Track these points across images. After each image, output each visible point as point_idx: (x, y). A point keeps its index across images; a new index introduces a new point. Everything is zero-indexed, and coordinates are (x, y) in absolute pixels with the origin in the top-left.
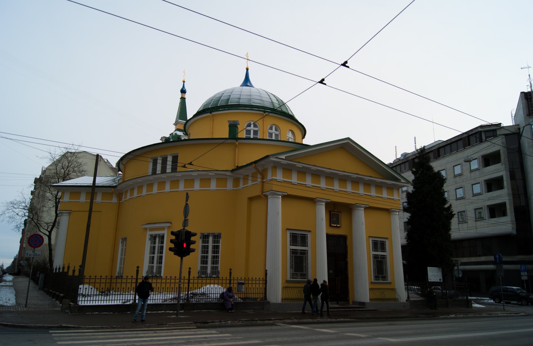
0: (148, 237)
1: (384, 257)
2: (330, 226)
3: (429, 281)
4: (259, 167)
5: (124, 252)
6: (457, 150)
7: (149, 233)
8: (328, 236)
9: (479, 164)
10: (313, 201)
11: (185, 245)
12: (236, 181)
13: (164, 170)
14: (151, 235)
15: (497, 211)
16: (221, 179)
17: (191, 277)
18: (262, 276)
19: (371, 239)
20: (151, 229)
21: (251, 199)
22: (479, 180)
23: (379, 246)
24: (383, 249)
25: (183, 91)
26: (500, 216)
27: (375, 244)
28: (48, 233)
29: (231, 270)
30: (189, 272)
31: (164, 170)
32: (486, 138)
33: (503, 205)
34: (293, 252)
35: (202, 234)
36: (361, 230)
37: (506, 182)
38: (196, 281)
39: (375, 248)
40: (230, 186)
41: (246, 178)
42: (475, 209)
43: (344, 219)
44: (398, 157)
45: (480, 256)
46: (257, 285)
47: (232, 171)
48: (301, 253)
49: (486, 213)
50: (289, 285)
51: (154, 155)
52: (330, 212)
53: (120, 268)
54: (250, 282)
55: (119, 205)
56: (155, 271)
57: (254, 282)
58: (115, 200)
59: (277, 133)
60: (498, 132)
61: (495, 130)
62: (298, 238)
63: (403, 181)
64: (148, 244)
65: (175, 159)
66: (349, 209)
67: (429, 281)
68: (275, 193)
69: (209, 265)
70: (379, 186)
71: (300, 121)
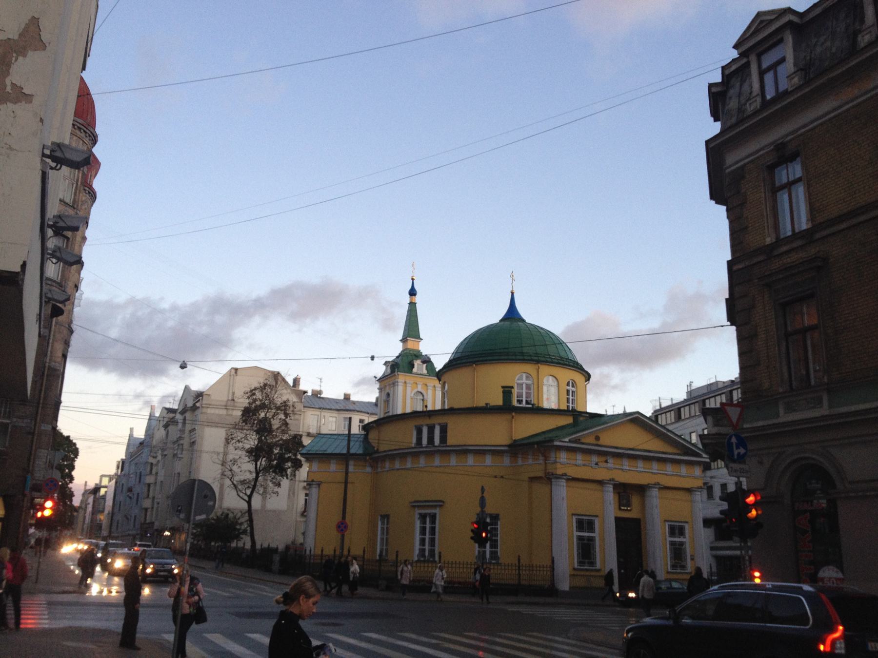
0: (417, 516)
2: (620, 509)
4: (541, 445)
5: (386, 531)
7: (418, 511)
8: (618, 520)
10: (601, 483)
11: (484, 535)
14: (420, 514)
16: (496, 452)
18: (549, 563)
21: (532, 479)
23: (677, 531)
25: (412, 292)
28: (246, 498)
31: (431, 440)
34: (580, 538)
36: (659, 512)
43: (635, 500)
47: (509, 446)
48: (584, 563)
50: (576, 573)
56: (427, 554)
62: (585, 524)
64: (418, 524)
66: (641, 490)
69: (427, 547)
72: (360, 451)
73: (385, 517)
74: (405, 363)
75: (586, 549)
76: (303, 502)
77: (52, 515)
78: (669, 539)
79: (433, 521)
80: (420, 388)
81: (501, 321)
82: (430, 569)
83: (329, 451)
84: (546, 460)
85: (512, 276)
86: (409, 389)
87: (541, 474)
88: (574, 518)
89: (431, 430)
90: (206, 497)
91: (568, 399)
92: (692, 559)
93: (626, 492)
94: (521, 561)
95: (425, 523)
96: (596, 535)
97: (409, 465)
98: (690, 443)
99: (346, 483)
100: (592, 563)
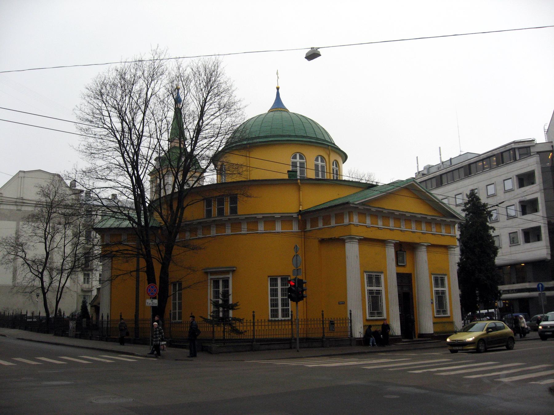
1: (379, 292)
3: (157, 305)
6: (491, 168)
7: (210, 277)
8: (398, 274)
9: (513, 185)
10: (383, 242)
15: (531, 235)
17: (256, 320)
19: (433, 276)
22: (513, 202)
23: (439, 282)
26: (535, 241)
29: (254, 312)
30: (254, 316)
31: (221, 212)
32: (520, 155)
33: (538, 229)
37: (541, 205)
39: (370, 283)
40: (295, 228)
42: (510, 234)
43: (407, 257)
44: (420, 170)
45: (514, 283)
46: (263, 327)
54: (263, 324)
57: (260, 324)
60: (532, 150)
61: (529, 147)
67: (157, 305)
68: (352, 238)
71: (342, 149)
75: (375, 301)
77: (494, 263)
78: (434, 289)
81: (271, 111)
82: (283, 327)
93: (405, 250)
94: (325, 316)
95: (218, 287)
96: (382, 288)
97: (403, 228)
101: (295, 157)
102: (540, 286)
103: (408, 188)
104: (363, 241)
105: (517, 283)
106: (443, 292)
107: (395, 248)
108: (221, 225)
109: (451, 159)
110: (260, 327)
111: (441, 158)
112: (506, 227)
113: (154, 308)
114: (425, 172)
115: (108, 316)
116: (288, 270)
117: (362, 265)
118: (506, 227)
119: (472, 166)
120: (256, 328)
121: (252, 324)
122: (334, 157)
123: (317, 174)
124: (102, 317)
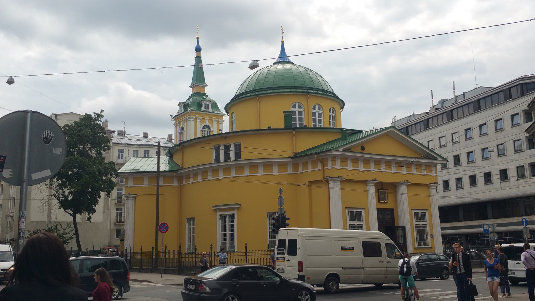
0: (218, 217)
1: (424, 226)
2: (379, 202)
4: (318, 155)
6: (499, 103)
7: (219, 213)
8: (378, 210)
12: (296, 166)
13: (227, 157)
14: (221, 215)
16: (282, 165)
17: (213, 253)
20: (220, 210)
23: (420, 217)
24: (424, 219)
25: (198, 50)
27: (417, 215)
29: (246, 244)
30: (246, 247)
31: (227, 157)
35: (268, 213)
38: (266, 253)
39: (417, 219)
40: (290, 171)
41: (305, 165)
43: (390, 197)
47: (292, 158)
49: (527, 171)
51: (217, 143)
52: (378, 190)
53: (189, 245)
55: (181, 187)
57: (251, 254)
58: (175, 183)
59: (320, 111)
63: (439, 159)
65: (238, 147)
66: (394, 186)
67: (49, 170)
68: (334, 179)
70: (419, 166)
72: (167, 169)
73: (191, 220)
74: (197, 103)
76: (116, 214)
79: (232, 221)
80: (207, 123)
83: (142, 170)
84: (324, 167)
85: (282, 28)
86: (199, 123)
87: (320, 178)
88: (347, 211)
89: (227, 148)
90: (47, 140)
91: (330, 122)
92: (432, 237)
95: (225, 222)
98: (428, 148)
99: (158, 195)
100: (425, 244)
101: (294, 107)
102: (524, 220)
103: (386, 134)
104: (345, 181)
105: (493, 218)
106: (424, 226)
107: (375, 187)
108: (227, 169)
109: (464, 93)
110: (251, 257)
111: (454, 92)
112: (514, 160)
113: (477, 294)
114: (439, 107)
115: (131, 249)
116: (275, 208)
117: (343, 203)
118: (514, 160)
119: (481, 101)
120: (248, 257)
121: (245, 254)
122: (327, 105)
123: (330, 125)
124: (126, 250)
